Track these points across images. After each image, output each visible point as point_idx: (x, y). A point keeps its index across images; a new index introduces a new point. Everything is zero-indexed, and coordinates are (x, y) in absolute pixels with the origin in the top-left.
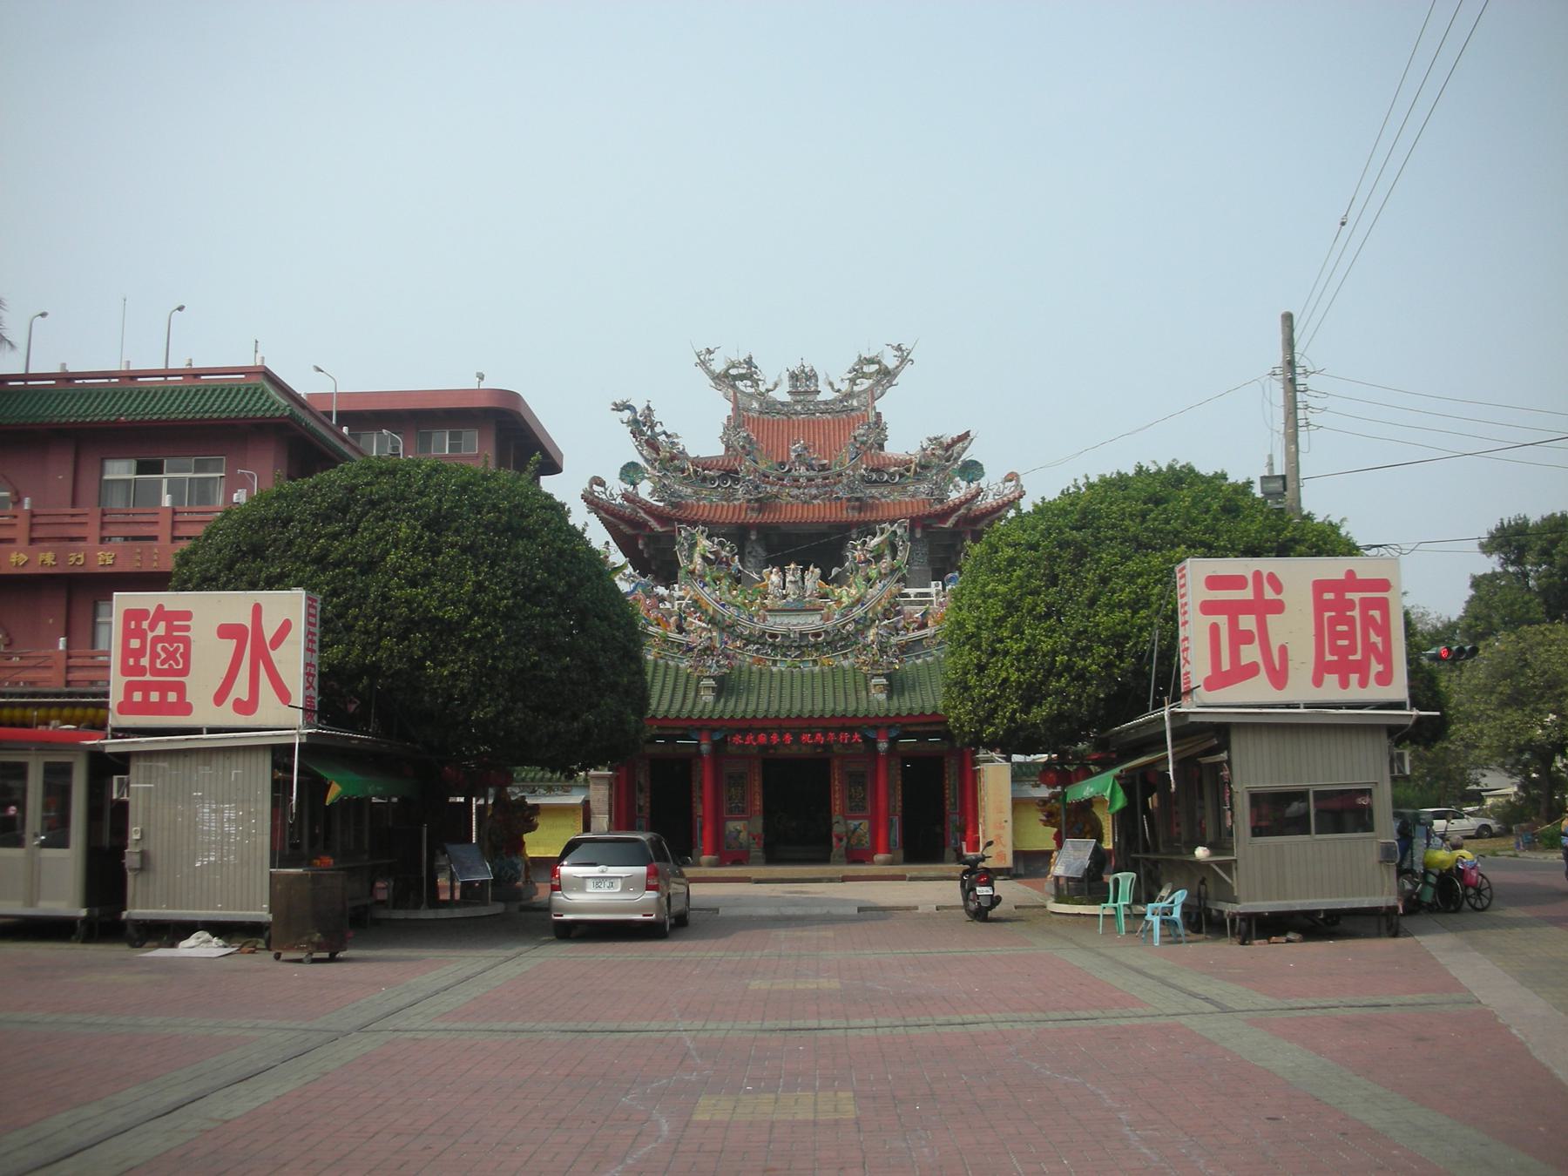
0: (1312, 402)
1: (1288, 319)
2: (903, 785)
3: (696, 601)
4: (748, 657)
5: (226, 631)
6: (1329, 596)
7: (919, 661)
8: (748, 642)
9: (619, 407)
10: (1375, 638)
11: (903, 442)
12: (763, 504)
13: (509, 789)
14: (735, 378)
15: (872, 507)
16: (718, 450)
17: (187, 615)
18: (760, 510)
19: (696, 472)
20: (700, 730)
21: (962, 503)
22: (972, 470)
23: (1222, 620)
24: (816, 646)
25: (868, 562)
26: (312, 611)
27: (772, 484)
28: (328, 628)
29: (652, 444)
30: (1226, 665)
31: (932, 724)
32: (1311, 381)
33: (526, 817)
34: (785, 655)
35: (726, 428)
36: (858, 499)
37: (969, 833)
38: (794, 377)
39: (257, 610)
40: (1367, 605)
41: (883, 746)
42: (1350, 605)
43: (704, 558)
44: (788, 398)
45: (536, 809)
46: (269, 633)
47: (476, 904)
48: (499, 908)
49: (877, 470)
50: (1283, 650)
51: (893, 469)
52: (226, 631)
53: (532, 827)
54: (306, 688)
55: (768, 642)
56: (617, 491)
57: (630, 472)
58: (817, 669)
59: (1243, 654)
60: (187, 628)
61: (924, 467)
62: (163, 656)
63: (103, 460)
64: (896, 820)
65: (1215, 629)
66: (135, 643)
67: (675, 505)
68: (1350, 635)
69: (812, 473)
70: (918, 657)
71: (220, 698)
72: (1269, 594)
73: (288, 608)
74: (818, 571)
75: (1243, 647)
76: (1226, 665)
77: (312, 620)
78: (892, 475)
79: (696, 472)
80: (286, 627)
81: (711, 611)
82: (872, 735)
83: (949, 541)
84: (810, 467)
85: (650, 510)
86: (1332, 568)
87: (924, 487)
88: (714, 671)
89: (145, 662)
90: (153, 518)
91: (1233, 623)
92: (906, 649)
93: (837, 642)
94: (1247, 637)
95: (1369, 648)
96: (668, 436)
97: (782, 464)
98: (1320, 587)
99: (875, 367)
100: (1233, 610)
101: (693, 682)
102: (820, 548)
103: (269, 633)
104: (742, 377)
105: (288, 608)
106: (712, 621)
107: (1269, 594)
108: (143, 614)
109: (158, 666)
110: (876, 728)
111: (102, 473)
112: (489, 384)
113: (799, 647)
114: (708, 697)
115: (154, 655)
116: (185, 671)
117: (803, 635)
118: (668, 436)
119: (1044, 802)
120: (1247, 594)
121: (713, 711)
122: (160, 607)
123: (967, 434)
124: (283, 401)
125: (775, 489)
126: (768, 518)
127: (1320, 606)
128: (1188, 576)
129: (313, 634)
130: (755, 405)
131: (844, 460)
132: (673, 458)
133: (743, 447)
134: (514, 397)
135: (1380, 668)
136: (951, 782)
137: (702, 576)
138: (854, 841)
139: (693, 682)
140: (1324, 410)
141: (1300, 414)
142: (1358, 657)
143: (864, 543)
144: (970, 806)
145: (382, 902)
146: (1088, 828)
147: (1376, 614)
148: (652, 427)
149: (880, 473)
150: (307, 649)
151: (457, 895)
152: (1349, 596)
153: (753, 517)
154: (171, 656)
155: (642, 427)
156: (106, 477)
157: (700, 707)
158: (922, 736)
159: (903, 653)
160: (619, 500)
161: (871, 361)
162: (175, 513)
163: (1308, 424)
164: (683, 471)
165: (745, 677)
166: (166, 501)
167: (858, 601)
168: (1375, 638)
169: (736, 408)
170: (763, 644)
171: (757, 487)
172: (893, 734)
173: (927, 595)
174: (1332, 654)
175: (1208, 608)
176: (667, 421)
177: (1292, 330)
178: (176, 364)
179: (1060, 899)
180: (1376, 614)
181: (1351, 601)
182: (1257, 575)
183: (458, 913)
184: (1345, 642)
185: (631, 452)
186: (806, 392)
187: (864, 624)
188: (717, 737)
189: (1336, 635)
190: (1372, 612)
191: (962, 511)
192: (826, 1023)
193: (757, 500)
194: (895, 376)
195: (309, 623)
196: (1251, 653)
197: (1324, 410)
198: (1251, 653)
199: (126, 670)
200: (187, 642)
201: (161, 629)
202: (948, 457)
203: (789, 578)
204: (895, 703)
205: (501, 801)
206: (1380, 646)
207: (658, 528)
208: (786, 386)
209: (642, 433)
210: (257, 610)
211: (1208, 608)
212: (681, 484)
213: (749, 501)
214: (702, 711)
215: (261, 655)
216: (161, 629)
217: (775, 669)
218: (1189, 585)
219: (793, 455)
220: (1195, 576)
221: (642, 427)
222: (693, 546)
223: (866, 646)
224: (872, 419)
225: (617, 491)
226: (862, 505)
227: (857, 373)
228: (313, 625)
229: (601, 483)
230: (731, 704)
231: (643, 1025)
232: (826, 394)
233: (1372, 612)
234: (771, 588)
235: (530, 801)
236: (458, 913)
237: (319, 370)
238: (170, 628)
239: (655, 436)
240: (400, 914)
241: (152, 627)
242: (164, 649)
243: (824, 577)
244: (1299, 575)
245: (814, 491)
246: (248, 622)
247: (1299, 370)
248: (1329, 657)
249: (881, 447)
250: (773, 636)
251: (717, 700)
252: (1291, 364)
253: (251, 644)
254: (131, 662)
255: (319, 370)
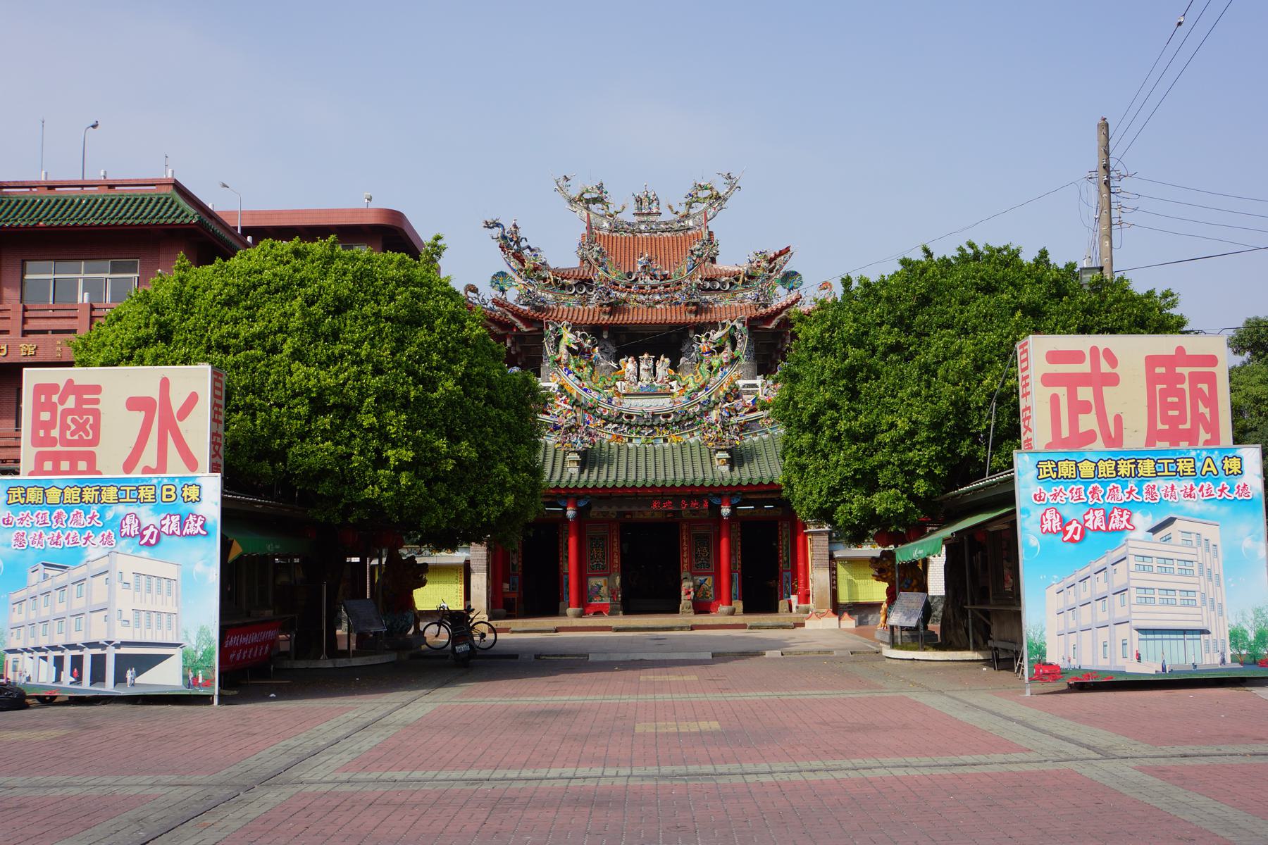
0: (1124, 202)
1: (1105, 126)
2: (742, 547)
3: (562, 387)
4: (607, 436)
5: (134, 404)
6: (1160, 370)
7: (756, 439)
8: (607, 421)
9: (488, 226)
10: (1202, 409)
11: (732, 259)
12: (615, 307)
13: (401, 551)
14: (588, 201)
15: (707, 311)
16: (574, 262)
17: (97, 389)
18: (610, 313)
19: (556, 281)
20: (566, 498)
21: (783, 308)
22: (790, 278)
23: (1062, 392)
24: (665, 426)
25: (711, 352)
26: (218, 385)
27: (621, 291)
28: (226, 401)
29: (518, 257)
30: (1065, 433)
31: (768, 492)
32: (1125, 184)
33: (419, 576)
34: (639, 433)
35: (581, 246)
36: (694, 304)
37: (801, 587)
38: (639, 201)
39: (165, 383)
40: (1195, 378)
41: (725, 511)
42: (1181, 379)
43: (568, 348)
44: (635, 219)
45: (425, 567)
46: (176, 405)
47: (371, 654)
48: (390, 657)
49: (711, 280)
50: (1118, 419)
51: (723, 279)
52: (134, 404)
53: (422, 584)
54: (212, 456)
55: (624, 420)
56: (488, 297)
57: (499, 279)
58: (667, 445)
59: (1081, 423)
60: (97, 401)
61: (751, 277)
62: (73, 427)
63: (23, 261)
64: (736, 576)
65: (1055, 399)
66: (45, 416)
67: (538, 309)
68: (1180, 406)
69: (654, 282)
70: (755, 435)
71: (129, 466)
72: (1105, 367)
73: (195, 380)
74: (667, 360)
75: (1081, 417)
76: (1065, 433)
77: (218, 393)
78: (723, 284)
79: (556, 281)
80: (193, 399)
81: (575, 395)
82: (716, 501)
83: (769, 342)
84: (654, 277)
85: (517, 314)
86: (1164, 344)
87: (750, 294)
88: (579, 446)
89: (55, 433)
90: (72, 314)
91: (1072, 395)
92: (744, 427)
93: (684, 421)
94: (1085, 407)
95: (1197, 417)
96: (532, 250)
97: (629, 275)
98: (1152, 361)
99: (707, 193)
100: (1073, 382)
101: (560, 454)
102: (669, 342)
103: (176, 405)
104: (595, 201)
105: (195, 380)
106: (575, 403)
107: (1105, 367)
108: (53, 388)
109: (69, 437)
110: (720, 496)
111: (23, 273)
112: (376, 205)
113: (651, 426)
114: (573, 470)
115: (64, 427)
116: (95, 441)
117: (654, 416)
118: (532, 250)
119: (874, 561)
120: (1085, 367)
121: (578, 481)
122: (70, 382)
123: (787, 249)
124: (191, 211)
125: (624, 295)
126: (619, 319)
127: (1152, 380)
128: (1031, 351)
129: (219, 406)
130: (606, 225)
131: (681, 270)
132: (535, 269)
133: (596, 260)
134: (397, 215)
135: (1208, 437)
136: (784, 542)
137: (567, 365)
138: (700, 594)
139: (560, 454)
140: (1135, 209)
141: (1115, 213)
142: (1188, 426)
143: (708, 336)
144: (801, 564)
145: (285, 653)
146: (915, 582)
147: (1205, 387)
148: (517, 242)
149: (712, 284)
150: (214, 420)
151: (353, 645)
152: (1179, 370)
153: (605, 319)
154: (81, 427)
155: (511, 244)
156: (27, 277)
157: (566, 477)
158: (759, 504)
159: (742, 431)
160: (490, 305)
161: (703, 188)
162: (92, 309)
163: (1121, 223)
164: (545, 279)
165: (605, 449)
166: (83, 298)
167: (703, 386)
168: (1202, 409)
169: (589, 227)
170: (620, 424)
171: (609, 294)
172: (735, 501)
173: (755, 386)
174: (1163, 423)
175: (1049, 380)
176: (531, 236)
177: (1108, 140)
178: (90, 176)
179: (894, 645)
180: (1205, 387)
181: (1182, 375)
182: (1094, 350)
183: (357, 662)
184: (1176, 413)
185: (499, 262)
186: (649, 214)
187: (708, 407)
188: (582, 504)
189: (1167, 406)
190: (1200, 386)
191: (784, 314)
192: (722, 768)
193: (608, 305)
194: (725, 200)
195: (214, 396)
196: (1088, 422)
197: (1135, 209)
198: (1088, 422)
199: (36, 441)
200: (96, 414)
201: (71, 402)
202: (774, 267)
203: (643, 366)
204: (736, 474)
205: (394, 558)
206: (1208, 416)
207: (524, 329)
208: (633, 207)
209: (509, 247)
210: (165, 383)
211: (1049, 380)
212: (543, 290)
213: (601, 305)
214: (569, 481)
215: (169, 426)
216: (71, 402)
217: (630, 445)
218: (1031, 360)
219: (639, 267)
220: (1037, 352)
221: (511, 244)
222: (559, 338)
223: (711, 425)
224: (706, 236)
225: (488, 297)
226: (699, 309)
227: (692, 199)
228: (220, 398)
229: (475, 290)
230: (594, 476)
231: (542, 772)
232: (667, 216)
233: (1200, 386)
234: (627, 375)
235: (419, 560)
236: (357, 662)
237: (225, 186)
238: (80, 401)
239: (520, 250)
240: (301, 664)
241: (62, 400)
242: (73, 421)
243: (674, 366)
244: (1132, 350)
245: (657, 297)
246: (155, 395)
247: (1112, 174)
248: (1160, 426)
249: (713, 261)
250: (630, 417)
251: (581, 471)
252: (1106, 168)
253: (159, 415)
254: (42, 433)
255: (225, 186)
